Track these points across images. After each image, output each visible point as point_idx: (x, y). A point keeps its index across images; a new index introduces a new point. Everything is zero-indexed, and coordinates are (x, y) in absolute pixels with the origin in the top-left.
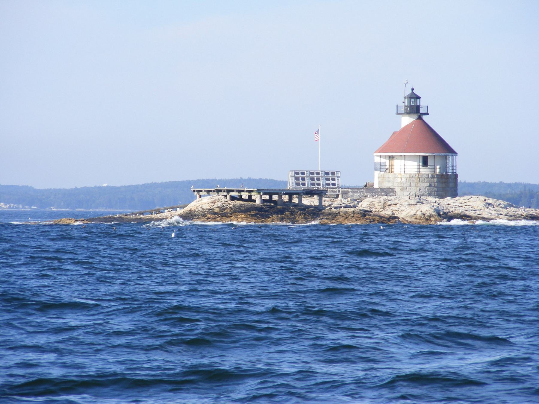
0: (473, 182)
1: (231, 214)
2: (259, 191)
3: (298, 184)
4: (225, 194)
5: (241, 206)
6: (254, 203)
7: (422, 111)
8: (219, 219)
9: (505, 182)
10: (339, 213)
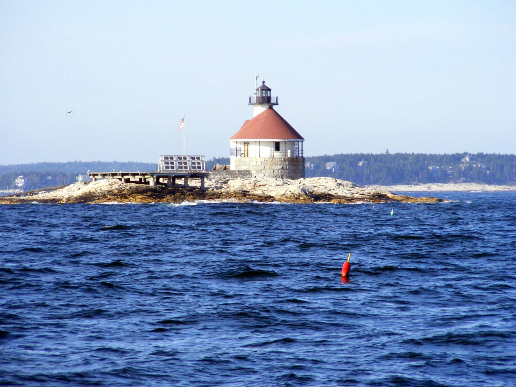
0: (88, 161)
1: (129, 195)
2: (152, 175)
3: (167, 168)
4: (120, 177)
5: (137, 187)
6: (147, 185)
7: (273, 101)
8: (119, 199)
9: (119, 161)
10: (221, 193)
